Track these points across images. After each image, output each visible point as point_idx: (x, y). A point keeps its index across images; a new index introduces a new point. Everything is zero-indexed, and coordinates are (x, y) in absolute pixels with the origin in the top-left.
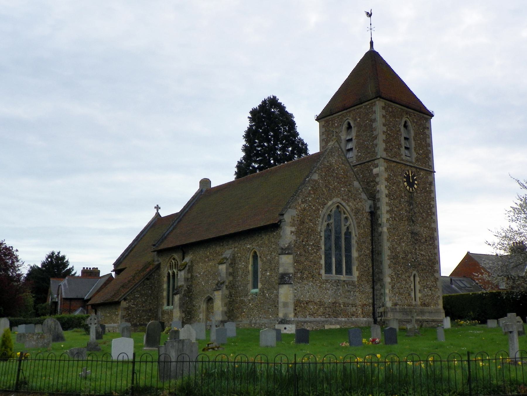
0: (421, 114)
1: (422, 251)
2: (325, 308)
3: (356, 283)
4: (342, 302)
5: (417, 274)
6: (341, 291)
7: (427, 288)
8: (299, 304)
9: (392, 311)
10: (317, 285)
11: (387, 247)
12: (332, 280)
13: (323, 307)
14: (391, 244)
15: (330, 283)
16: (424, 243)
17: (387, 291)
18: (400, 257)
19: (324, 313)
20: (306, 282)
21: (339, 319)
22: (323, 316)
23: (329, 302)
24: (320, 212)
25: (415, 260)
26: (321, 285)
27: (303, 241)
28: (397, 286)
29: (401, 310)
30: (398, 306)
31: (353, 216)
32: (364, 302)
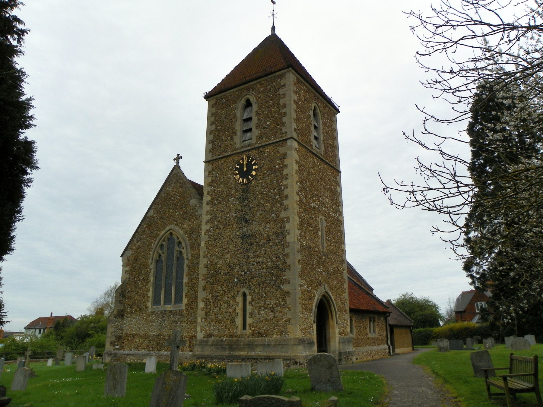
0: (269, 76)
1: (259, 257)
2: (150, 341)
3: (185, 312)
4: (167, 334)
5: (247, 292)
6: (166, 323)
7: (266, 308)
8: (127, 337)
9: (200, 345)
10: (143, 318)
11: (203, 265)
12: (158, 311)
13: (147, 340)
14: (209, 260)
15: (156, 315)
16: (263, 245)
17: (199, 320)
18: (222, 273)
19: (148, 346)
20: (134, 316)
21: (162, 352)
22: (146, 349)
23: (154, 335)
24: (153, 245)
25: (245, 273)
26: (147, 318)
27: (135, 278)
28: (213, 312)
29: (215, 343)
30: (213, 337)
31: (186, 237)
32: (192, 334)
